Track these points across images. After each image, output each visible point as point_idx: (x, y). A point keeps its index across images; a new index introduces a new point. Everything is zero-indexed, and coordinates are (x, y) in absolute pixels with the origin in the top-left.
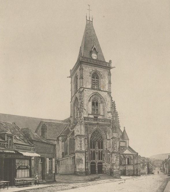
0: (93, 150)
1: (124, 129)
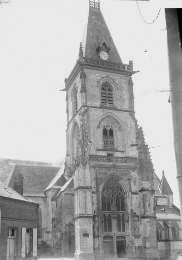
0: (107, 213)
1: (163, 174)
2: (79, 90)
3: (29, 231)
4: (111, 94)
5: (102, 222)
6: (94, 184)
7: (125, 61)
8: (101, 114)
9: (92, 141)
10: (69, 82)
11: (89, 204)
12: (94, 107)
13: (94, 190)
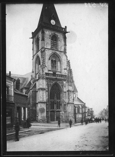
2: (40, 39)
3: (24, 109)
4: (52, 43)
5: (50, 105)
6: (47, 87)
7: (63, 26)
8: (51, 52)
9: (46, 66)
10: (35, 34)
11: (45, 96)
12: (48, 49)
13: (47, 90)
